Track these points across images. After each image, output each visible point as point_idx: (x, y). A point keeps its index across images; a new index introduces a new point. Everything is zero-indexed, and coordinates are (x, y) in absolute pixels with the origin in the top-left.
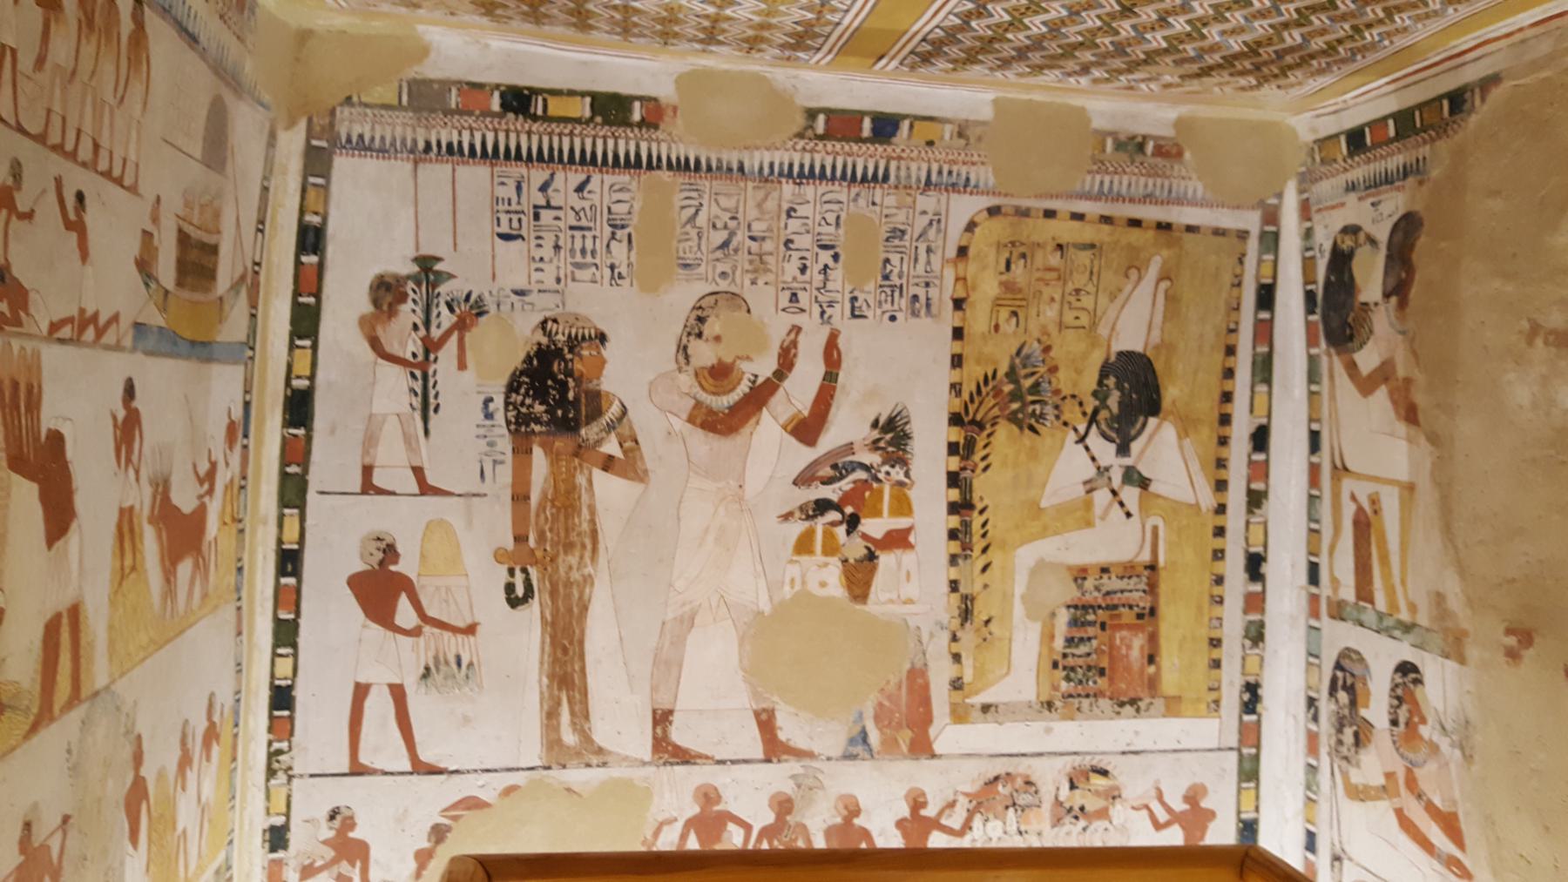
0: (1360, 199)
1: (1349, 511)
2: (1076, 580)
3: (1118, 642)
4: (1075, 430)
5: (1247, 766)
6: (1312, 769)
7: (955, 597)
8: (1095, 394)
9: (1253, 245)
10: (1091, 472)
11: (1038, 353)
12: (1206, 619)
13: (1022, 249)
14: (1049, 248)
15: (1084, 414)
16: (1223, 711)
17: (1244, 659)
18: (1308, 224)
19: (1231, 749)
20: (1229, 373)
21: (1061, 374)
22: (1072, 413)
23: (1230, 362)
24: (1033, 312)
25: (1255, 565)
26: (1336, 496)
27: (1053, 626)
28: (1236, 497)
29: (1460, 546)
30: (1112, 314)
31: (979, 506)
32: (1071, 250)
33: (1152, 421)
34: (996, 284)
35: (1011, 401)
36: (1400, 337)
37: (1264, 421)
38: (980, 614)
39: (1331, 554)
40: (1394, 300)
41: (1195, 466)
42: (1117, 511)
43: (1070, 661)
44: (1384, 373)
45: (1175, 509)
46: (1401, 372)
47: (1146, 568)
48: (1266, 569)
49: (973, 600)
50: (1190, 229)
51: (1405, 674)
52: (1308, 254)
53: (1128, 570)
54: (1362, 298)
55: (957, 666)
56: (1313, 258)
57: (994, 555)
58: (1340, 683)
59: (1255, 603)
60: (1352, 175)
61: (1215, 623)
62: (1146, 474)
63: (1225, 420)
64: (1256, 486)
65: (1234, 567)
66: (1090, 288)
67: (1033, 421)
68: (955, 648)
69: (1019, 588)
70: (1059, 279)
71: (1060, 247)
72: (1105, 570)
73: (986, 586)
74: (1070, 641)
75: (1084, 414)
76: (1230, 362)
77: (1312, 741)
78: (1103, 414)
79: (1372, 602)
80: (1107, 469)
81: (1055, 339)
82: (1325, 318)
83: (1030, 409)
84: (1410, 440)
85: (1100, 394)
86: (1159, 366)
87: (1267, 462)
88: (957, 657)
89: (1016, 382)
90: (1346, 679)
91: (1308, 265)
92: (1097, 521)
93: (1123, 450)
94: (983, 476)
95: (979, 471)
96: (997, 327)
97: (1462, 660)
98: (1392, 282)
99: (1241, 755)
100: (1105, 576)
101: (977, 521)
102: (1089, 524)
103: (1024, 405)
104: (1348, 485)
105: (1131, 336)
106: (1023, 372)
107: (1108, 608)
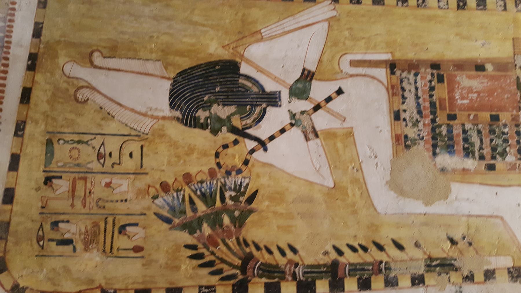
2: (407, 147)
3: (466, 102)
4: (252, 151)
7: (430, 279)
8: (215, 132)
10: (296, 133)
11: (169, 199)
12: (440, 12)
13: (47, 227)
14: (48, 193)
15: (236, 142)
21: (193, 170)
22: (234, 157)
24: (121, 207)
27: (454, 170)
30: (127, 117)
31: (334, 255)
32: (53, 167)
33: (245, 69)
34: (87, 255)
35: (221, 225)
38: (444, 250)
41: (290, 23)
42: (336, 105)
43: (487, 151)
45: (331, 43)
47: (393, 73)
49: (431, 259)
50: (37, 33)
53: (396, 91)
55: (497, 275)
57: (385, 236)
62: (298, 75)
66: (96, 143)
67: (243, 199)
68: (479, 277)
69: (416, 207)
70: (85, 179)
71: (48, 181)
72: (397, 116)
73: (417, 245)
74: (468, 152)
75: (236, 142)
78: (237, 122)
80: (293, 116)
81: (154, 178)
83: (230, 202)
85: (215, 126)
86: (186, 63)
88: (489, 275)
89: (200, 221)
92: (346, 125)
93: (273, 99)
94: (302, 253)
95: (296, 258)
96: (137, 249)
100: (403, 115)
101: (350, 257)
102: (350, 134)
103: (226, 209)
105: (155, 96)
106: (189, 213)
107: (433, 113)
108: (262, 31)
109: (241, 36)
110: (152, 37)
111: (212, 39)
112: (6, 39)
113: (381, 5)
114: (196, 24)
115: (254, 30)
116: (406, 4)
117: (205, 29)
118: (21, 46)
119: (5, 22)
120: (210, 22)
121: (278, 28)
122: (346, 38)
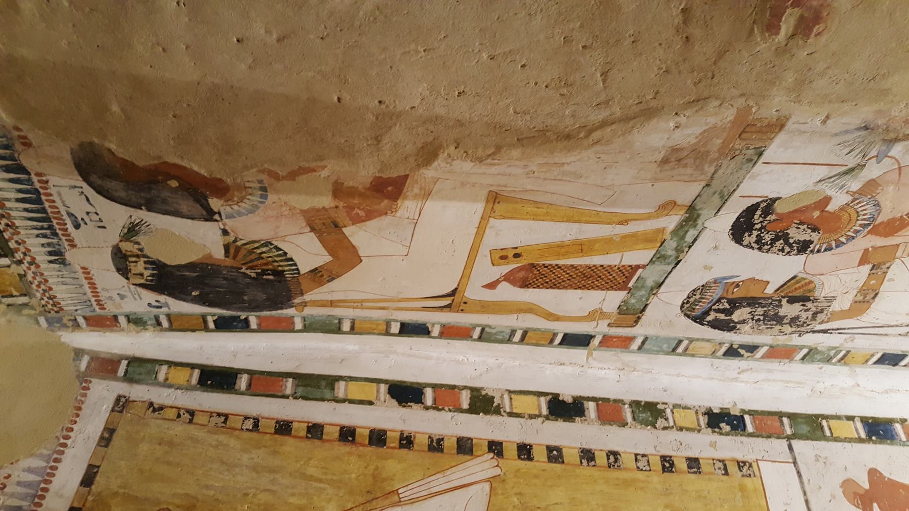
0: (73, 246)
1: (508, 292)
5: (805, 429)
6: (811, 355)
9: (139, 392)
12: (640, 475)
16: (749, 458)
17: (681, 429)
18: (122, 320)
19: (790, 447)
20: (315, 431)
23: (300, 429)
25: (564, 409)
26: (485, 307)
28: (480, 428)
29: (603, 114)
36: (272, 197)
37: (383, 388)
39: (558, 318)
40: (215, 203)
41: (438, 482)
44: (327, 228)
46: (326, 201)
48: (567, 394)
50: (88, 480)
51: (750, 228)
52: (165, 324)
54: (219, 254)
56: (169, 317)
58: (722, 316)
59: (610, 411)
60: (42, 258)
61: (642, 463)
63: (378, 438)
64: (465, 400)
65: (570, 435)
76: (300, 429)
77: (780, 353)
79: (635, 269)
82: (255, 307)
84: (426, 195)
87: (435, 387)
90: (717, 309)
91: (178, 324)
97: (779, 125)
98: (186, 205)
99: (794, 436)
104: (474, 292)
108: (400, 491)
109: (370, 497)
110: (246, 495)
111: (330, 500)
112: (42, 485)
113: (559, 463)
114: (311, 478)
115: (390, 489)
116: (593, 463)
117: (322, 485)
118: (61, 496)
119: (48, 463)
120: (329, 477)
121: (422, 488)
122: (514, 506)
